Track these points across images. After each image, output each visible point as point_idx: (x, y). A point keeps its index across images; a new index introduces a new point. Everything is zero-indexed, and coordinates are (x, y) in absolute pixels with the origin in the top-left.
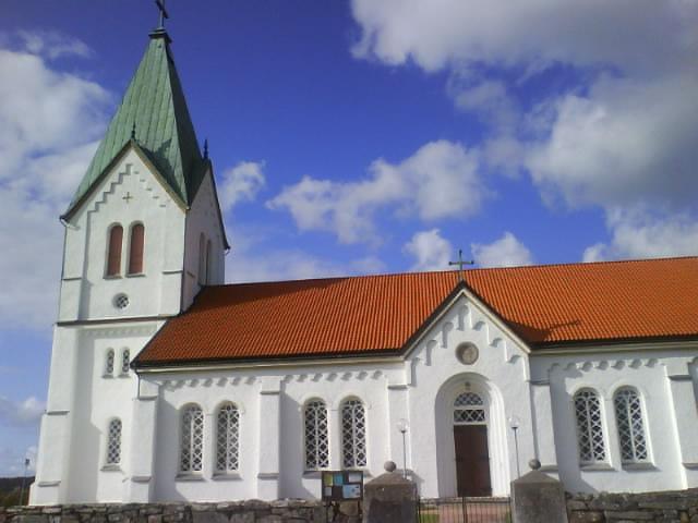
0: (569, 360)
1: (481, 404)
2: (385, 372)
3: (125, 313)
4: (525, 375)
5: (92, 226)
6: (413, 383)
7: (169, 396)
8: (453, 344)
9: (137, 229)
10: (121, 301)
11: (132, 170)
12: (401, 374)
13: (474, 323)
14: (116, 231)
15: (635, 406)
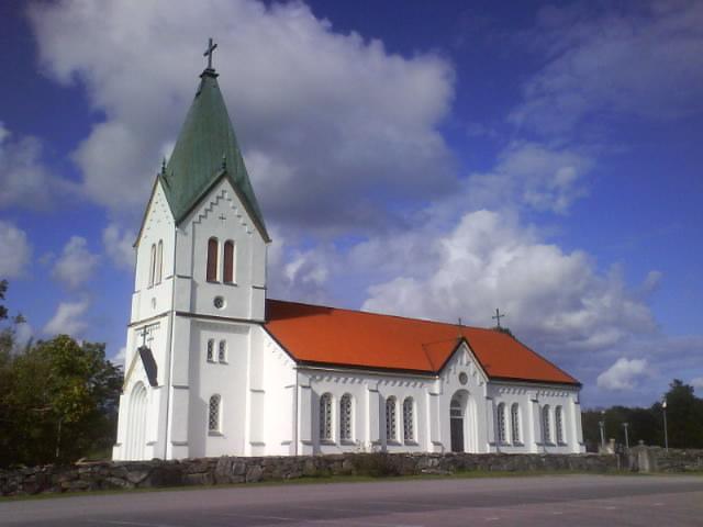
0: (497, 387)
1: (459, 406)
2: (426, 384)
3: (224, 311)
4: (485, 395)
5: (197, 234)
6: (441, 393)
7: (315, 387)
8: (458, 373)
9: (229, 245)
10: (218, 302)
11: (226, 196)
12: (436, 386)
13: (466, 362)
14: (213, 242)
15: (329, 405)
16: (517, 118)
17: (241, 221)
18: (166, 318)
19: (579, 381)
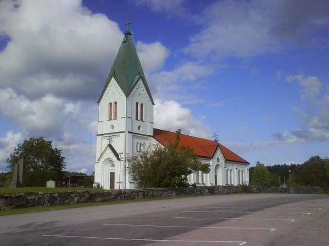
9: (142, 105)
10: (139, 128)
14: (137, 104)
16: (186, 50)
17: (118, 91)
18: (123, 134)
19: (249, 162)
